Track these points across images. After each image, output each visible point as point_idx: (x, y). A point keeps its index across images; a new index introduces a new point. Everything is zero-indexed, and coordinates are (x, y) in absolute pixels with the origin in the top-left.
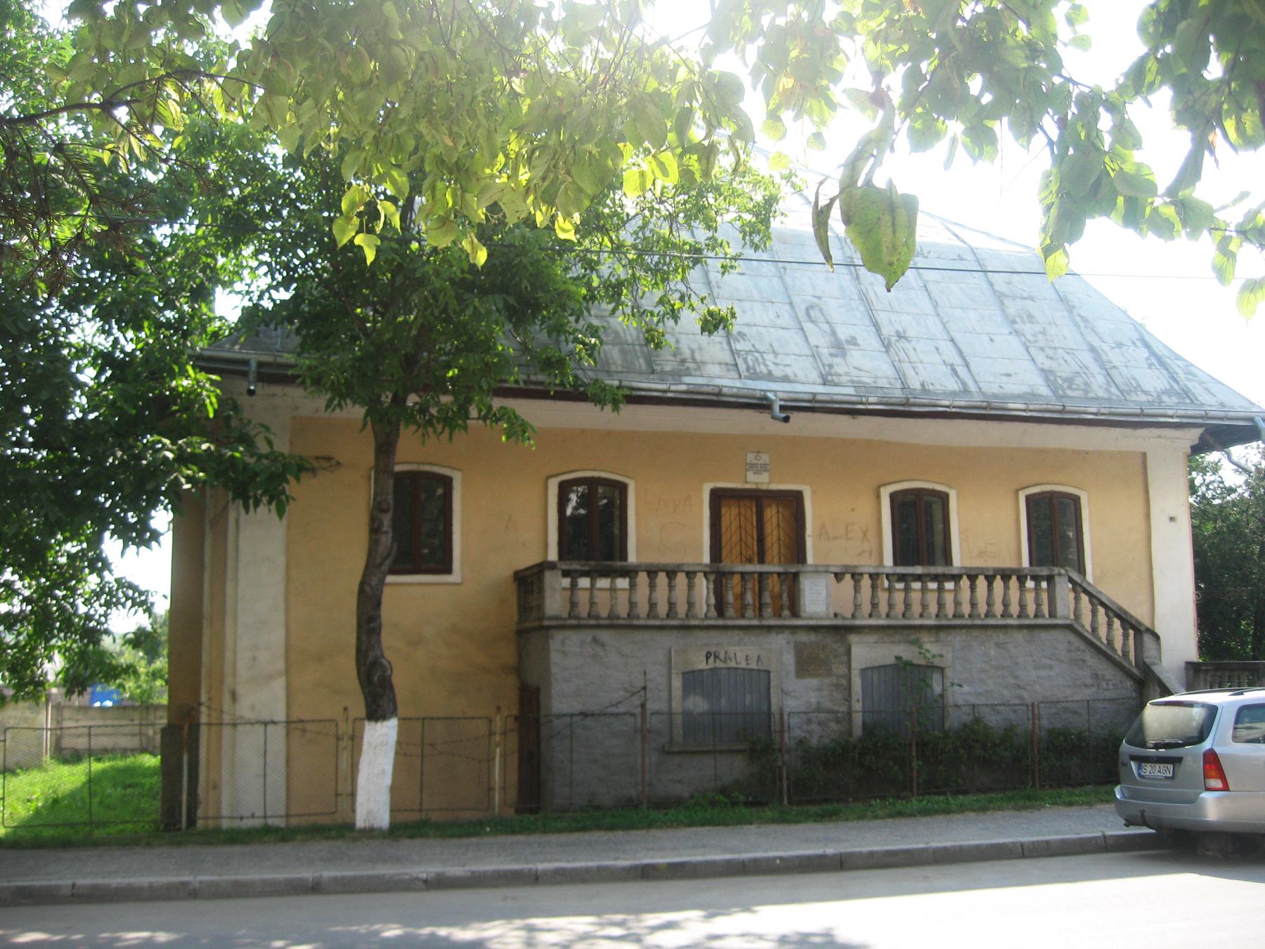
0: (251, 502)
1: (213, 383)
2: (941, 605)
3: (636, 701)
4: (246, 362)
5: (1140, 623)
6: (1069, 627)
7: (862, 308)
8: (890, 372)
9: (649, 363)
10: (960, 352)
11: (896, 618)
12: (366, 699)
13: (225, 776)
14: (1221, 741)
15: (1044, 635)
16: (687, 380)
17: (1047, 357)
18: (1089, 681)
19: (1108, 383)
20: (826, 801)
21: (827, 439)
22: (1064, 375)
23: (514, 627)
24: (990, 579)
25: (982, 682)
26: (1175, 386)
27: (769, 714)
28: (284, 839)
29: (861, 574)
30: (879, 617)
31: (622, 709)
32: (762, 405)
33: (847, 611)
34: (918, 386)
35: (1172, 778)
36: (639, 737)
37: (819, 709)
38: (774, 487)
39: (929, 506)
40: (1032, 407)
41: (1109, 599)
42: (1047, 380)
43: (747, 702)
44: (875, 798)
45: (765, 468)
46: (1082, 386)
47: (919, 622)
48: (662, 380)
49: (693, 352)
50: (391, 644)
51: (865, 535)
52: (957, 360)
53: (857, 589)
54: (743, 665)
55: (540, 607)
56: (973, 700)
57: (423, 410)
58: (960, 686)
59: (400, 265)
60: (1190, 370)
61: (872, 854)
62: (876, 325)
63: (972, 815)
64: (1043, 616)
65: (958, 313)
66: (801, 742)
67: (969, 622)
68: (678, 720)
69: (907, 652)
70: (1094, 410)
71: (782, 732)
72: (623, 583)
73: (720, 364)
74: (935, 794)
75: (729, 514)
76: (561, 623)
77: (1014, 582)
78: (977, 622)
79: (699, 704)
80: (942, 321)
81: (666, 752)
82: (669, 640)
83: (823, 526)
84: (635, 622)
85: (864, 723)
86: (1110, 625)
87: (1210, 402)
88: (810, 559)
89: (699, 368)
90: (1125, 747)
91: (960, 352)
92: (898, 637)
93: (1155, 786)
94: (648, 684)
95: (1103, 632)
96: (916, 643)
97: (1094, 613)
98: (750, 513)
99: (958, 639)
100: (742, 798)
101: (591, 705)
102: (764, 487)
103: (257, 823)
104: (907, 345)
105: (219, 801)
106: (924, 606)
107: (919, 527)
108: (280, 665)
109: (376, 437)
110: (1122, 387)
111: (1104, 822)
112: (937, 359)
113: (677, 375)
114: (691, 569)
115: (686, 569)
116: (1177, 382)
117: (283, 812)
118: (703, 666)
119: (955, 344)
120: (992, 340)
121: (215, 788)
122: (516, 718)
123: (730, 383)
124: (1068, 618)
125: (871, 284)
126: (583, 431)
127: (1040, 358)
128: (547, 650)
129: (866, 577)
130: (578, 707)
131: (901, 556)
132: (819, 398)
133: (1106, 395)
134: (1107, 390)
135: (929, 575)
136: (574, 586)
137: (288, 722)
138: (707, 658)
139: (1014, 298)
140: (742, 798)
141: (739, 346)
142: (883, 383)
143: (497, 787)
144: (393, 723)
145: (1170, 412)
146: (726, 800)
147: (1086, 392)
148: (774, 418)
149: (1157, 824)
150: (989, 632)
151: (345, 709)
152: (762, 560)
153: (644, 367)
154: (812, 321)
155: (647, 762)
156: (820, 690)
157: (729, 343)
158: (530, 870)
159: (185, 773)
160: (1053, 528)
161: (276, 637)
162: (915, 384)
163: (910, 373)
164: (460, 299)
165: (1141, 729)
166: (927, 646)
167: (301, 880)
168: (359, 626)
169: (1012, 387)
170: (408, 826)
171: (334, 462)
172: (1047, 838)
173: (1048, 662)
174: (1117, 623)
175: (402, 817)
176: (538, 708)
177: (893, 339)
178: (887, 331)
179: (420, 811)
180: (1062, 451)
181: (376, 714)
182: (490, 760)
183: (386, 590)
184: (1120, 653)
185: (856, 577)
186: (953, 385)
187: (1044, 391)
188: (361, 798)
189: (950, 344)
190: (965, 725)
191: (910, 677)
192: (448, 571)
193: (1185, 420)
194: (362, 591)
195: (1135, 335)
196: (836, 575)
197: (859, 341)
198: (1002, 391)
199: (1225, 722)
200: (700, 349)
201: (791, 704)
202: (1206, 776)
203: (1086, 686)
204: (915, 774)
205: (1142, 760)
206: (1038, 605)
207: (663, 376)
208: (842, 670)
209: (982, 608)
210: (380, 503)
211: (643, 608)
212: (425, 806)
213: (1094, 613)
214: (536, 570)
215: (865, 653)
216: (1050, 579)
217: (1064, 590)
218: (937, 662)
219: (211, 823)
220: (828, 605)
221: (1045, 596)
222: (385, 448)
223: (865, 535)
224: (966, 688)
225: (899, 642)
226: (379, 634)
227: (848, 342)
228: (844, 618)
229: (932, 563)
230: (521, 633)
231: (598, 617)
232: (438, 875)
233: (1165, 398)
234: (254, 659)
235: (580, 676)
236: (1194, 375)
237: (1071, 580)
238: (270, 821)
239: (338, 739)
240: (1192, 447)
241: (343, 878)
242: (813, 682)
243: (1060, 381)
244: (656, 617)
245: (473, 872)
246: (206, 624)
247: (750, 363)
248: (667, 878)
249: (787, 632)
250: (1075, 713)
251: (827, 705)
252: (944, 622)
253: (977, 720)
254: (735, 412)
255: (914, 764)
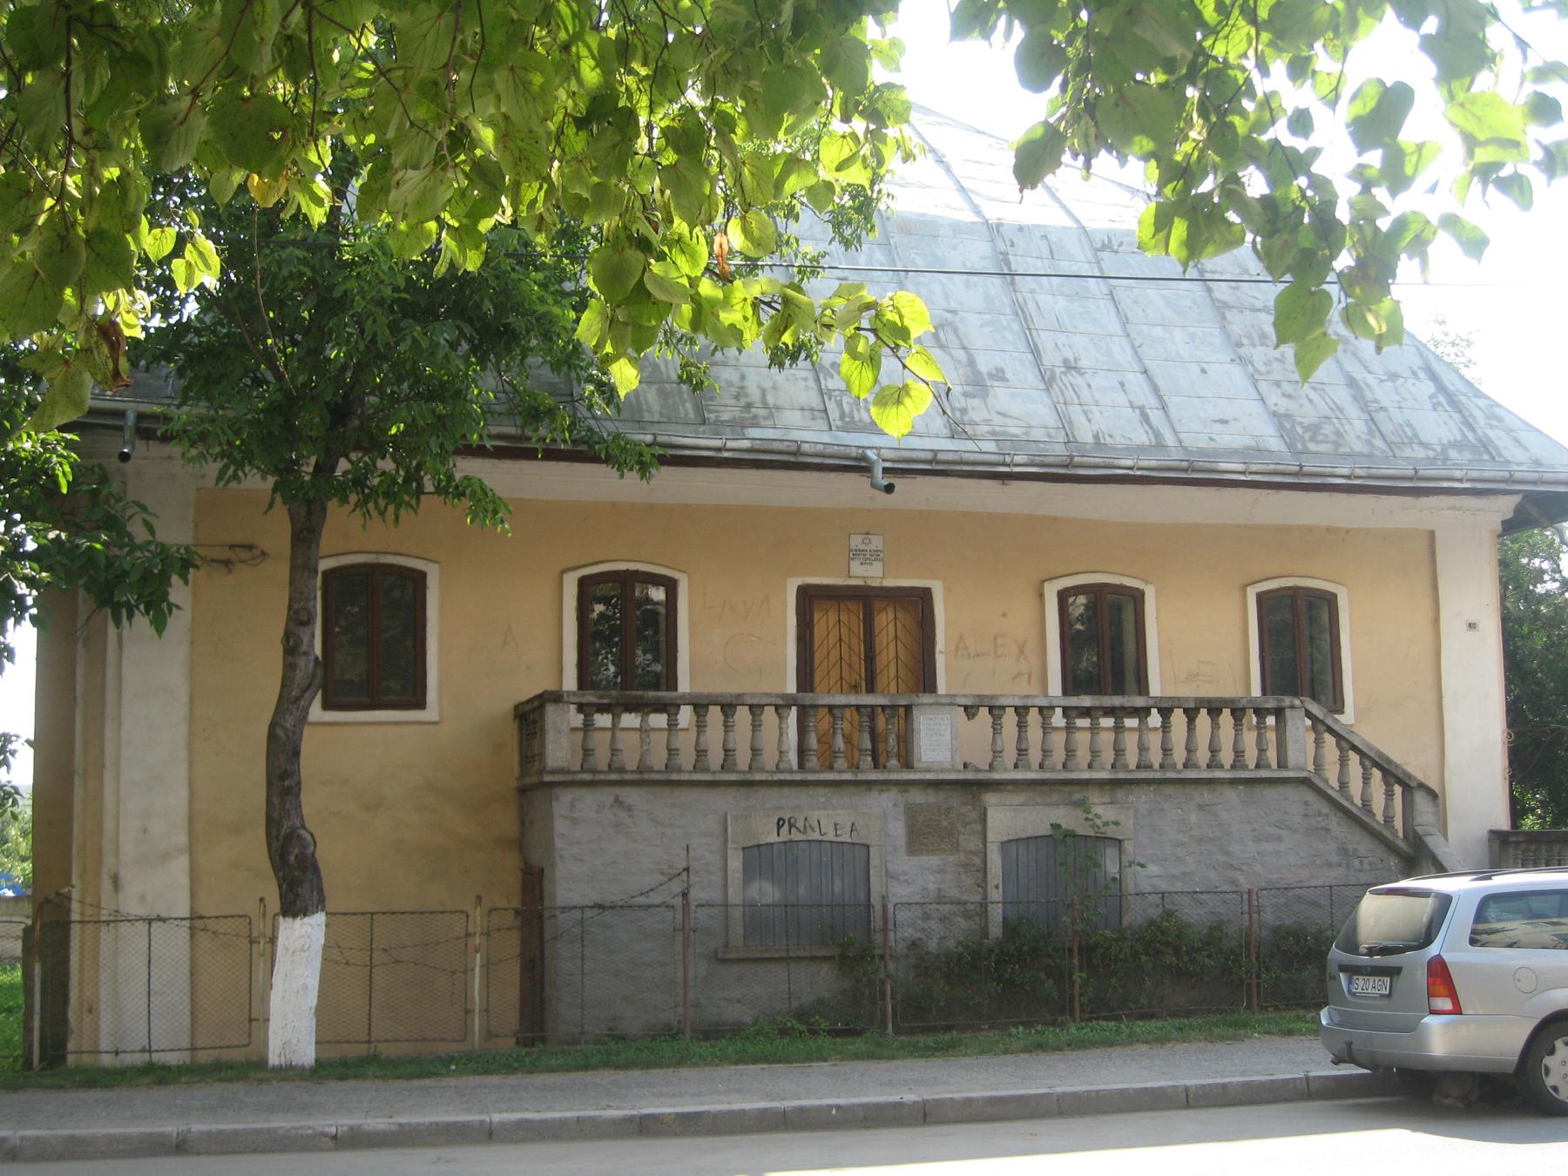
0: (124, 611)
1: (69, 445)
2: (1119, 751)
3: (677, 887)
4: (121, 414)
5: (1410, 776)
6: (1305, 782)
7: (1016, 327)
8: (1051, 420)
9: (699, 409)
10: (1156, 389)
11: (1053, 770)
12: (280, 886)
13: (105, 994)
14: (1450, 946)
15: (1270, 793)
16: (754, 433)
17: (1284, 395)
18: (1334, 859)
19: (1370, 432)
20: (947, 1029)
21: (966, 515)
22: (1306, 421)
23: (514, 784)
24: (1191, 714)
25: (1169, 861)
26: (1470, 435)
27: (869, 905)
28: (162, 1082)
29: (1003, 708)
30: (1028, 768)
31: (655, 899)
32: (860, 466)
33: (982, 759)
34: (1090, 440)
35: (1390, 995)
36: (679, 939)
37: (940, 900)
38: (890, 583)
39: (1119, 608)
40: (1254, 468)
41: (1364, 741)
42: (1280, 427)
43: (837, 890)
44: (1016, 1025)
45: (876, 555)
46: (1332, 437)
47: (1085, 775)
48: (717, 434)
49: (763, 392)
50: (313, 803)
51: (1021, 652)
52: (1152, 401)
53: (996, 728)
54: (831, 836)
55: (542, 755)
56: (1164, 886)
57: (359, 482)
58: (1142, 866)
59: (312, 281)
60: (1494, 413)
61: (969, 1101)
62: (1035, 351)
63: (1144, 1048)
64: (1268, 767)
65: (1158, 332)
66: (914, 944)
67: (1158, 775)
68: (737, 914)
69: (1068, 818)
70: (1345, 472)
71: (885, 930)
72: (659, 720)
73: (802, 409)
74: (1106, 1019)
75: (825, 622)
76: (569, 778)
77: (1226, 717)
78: (1171, 775)
79: (766, 892)
80: (1132, 346)
81: (720, 960)
82: (724, 801)
83: (961, 637)
84: (675, 777)
85: (1005, 918)
86: (1366, 779)
87: (1518, 459)
88: (942, 688)
89: (771, 416)
90: (1336, 954)
91: (1156, 389)
92: (1055, 797)
93: (1369, 1007)
94: (694, 865)
95: (1355, 787)
96: (1082, 805)
97: (1343, 761)
98: (852, 618)
99: (1142, 799)
100: (824, 1025)
101: (612, 894)
102: (875, 583)
103: (139, 1059)
104: (1078, 380)
105: (96, 1030)
106: (1095, 753)
107: (1103, 645)
108: (182, 839)
109: (292, 520)
110: (1391, 438)
111: (1309, 1060)
112: (1122, 399)
113: (739, 425)
114: (755, 702)
115: (749, 702)
116: (1473, 430)
117: (186, 1043)
118: (773, 838)
119: (1149, 378)
120: (1204, 371)
121: (90, 1011)
122: (517, 913)
123: (814, 436)
124: (1303, 769)
125: (1032, 292)
126: (613, 505)
127: (1274, 398)
128: (549, 815)
129: (1010, 712)
130: (595, 897)
131: (1072, 684)
132: (941, 456)
133: (1366, 450)
134: (1368, 442)
135: (1101, 708)
136: (588, 726)
137: (194, 917)
138: (779, 827)
139: (1241, 309)
140: (824, 1025)
141: (831, 384)
142: (1039, 434)
143: (477, 1008)
144: (319, 919)
145: (1458, 474)
146: (802, 1028)
147: (1337, 445)
148: (874, 486)
149: (1373, 1064)
150: (1189, 789)
151: (262, 900)
152: (871, 689)
153: (691, 414)
154: (942, 347)
155: (691, 974)
156: (942, 871)
157: (818, 380)
158: (482, 1122)
159: (37, 989)
160: (1298, 643)
161: (177, 799)
162: (1085, 435)
163: (1078, 418)
164: (394, 328)
165: (1354, 929)
166: (1099, 810)
167: (161, 1135)
168: (269, 783)
169: (1228, 439)
170: (339, 1066)
171: (256, 552)
172: (1225, 1080)
173: (1276, 831)
174: (1377, 774)
175: (333, 1053)
176: (542, 899)
177: (1058, 371)
178: (1051, 359)
179: (369, 1042)
180: (1311, 529)
181: (293, 907)
182: (467, 971)
183: (307, 731)
184: (1380, 818)
185: (996, 711)
186: (1141, 437)
187: (1275, 444)
188: (274, 1025)
189: (1141, 377)
190: (1152, 922)
191: (1071, 853)
192: (420, 704)
193: (1479, 486)
194: (272, 736)
195: (1417, 362)
196: (966, 708)
197: (1008, 375)
198: (1212, 445)
199: (1460, 921)
200: (774, 388)
201: (900, 892)
202: (1431, 995)
203: (1330, 865)
204: (1077, 990)
205: (1353, 971)
206: (1262, 751)
207: (717, 427)
208: (973, 843)
209: (1179, 755)
210: (297, 612)
211: (687, 758)
212: (374, 1036)
213: (1343, 761)
214: (536, 703)
215: (1006, 819)
216: (1279, 712)
217: (1299, 728)
218: (1111, 831)
219: (86, 1059)
220: (953, 752)
221: (1271, 736)
222: (305, 536)
223: (1021, 652)
224: (1153, 869)
225: (1057, 805)
226: (298, 796)
227: (991, 376)
228: (978, 770)
229: (1120, 690)
230: (523, 791)
231: (622, 770)
232: (352, 1128)
233: (1453, 453)
234: (145, 830)
235: (601, 853)
236: (1500, 420)
237: (1309, 714)
238: (156, 1057)
239: (251, 942)
240: (1504, 522)
241: (220, 1132)
242: (934, 861)
243: (1299, 430)
244: (706, 770)
245: (401, 1125)
246: (77, 780)
247: (846, 408)
248: (676, 1135)
249: (894, 790)
250: (1313, 903)
251: (954, 893)
252: (1121, 775)
253: (1168, 914)
254: (833, 475)
255: (1075, 977)
